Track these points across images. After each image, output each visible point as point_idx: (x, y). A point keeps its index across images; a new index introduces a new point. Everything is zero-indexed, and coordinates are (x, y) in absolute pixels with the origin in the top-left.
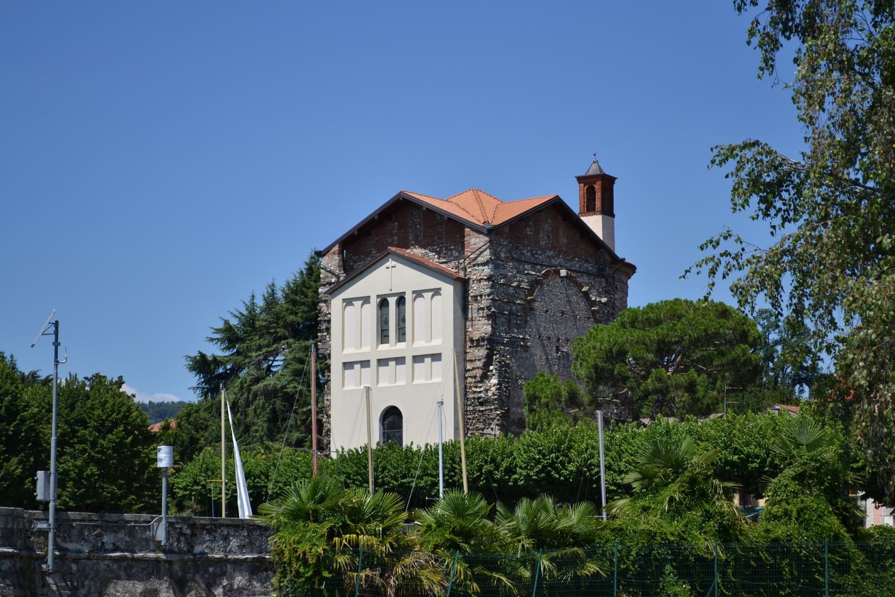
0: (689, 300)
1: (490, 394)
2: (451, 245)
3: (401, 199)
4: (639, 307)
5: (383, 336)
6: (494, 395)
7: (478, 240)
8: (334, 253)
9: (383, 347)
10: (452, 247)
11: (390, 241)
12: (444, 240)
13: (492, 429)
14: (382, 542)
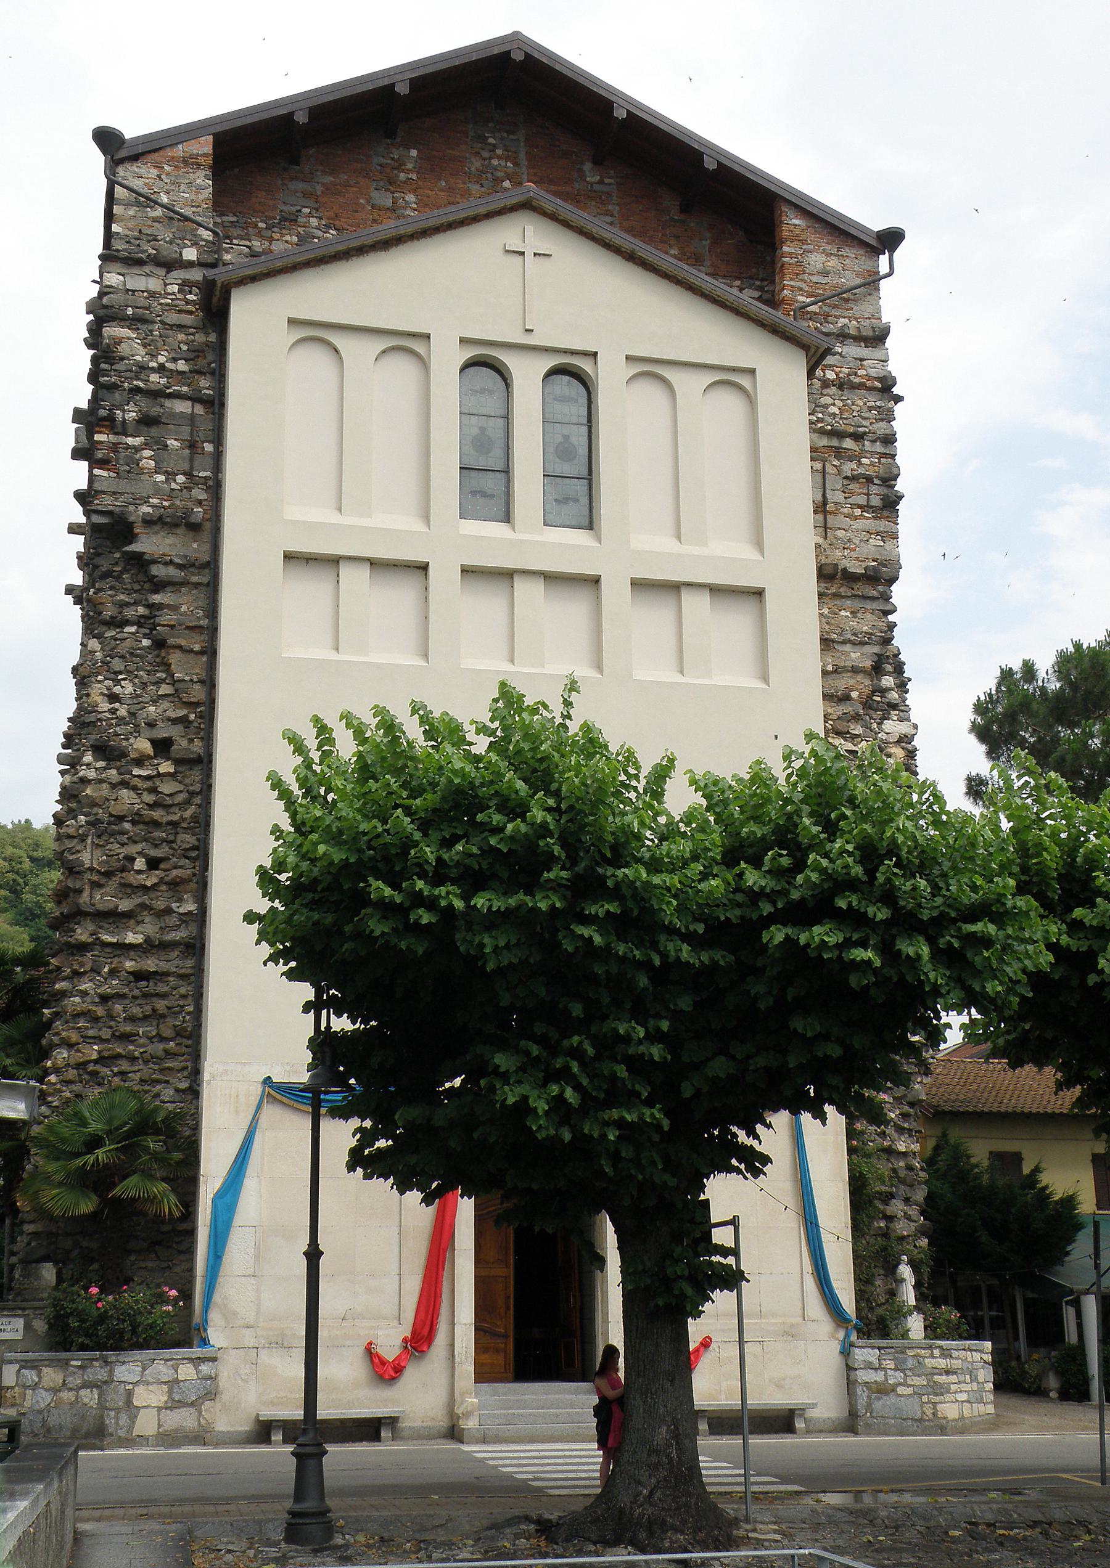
3: (518, 56)
7: (833, 263)
8: (190, 162)
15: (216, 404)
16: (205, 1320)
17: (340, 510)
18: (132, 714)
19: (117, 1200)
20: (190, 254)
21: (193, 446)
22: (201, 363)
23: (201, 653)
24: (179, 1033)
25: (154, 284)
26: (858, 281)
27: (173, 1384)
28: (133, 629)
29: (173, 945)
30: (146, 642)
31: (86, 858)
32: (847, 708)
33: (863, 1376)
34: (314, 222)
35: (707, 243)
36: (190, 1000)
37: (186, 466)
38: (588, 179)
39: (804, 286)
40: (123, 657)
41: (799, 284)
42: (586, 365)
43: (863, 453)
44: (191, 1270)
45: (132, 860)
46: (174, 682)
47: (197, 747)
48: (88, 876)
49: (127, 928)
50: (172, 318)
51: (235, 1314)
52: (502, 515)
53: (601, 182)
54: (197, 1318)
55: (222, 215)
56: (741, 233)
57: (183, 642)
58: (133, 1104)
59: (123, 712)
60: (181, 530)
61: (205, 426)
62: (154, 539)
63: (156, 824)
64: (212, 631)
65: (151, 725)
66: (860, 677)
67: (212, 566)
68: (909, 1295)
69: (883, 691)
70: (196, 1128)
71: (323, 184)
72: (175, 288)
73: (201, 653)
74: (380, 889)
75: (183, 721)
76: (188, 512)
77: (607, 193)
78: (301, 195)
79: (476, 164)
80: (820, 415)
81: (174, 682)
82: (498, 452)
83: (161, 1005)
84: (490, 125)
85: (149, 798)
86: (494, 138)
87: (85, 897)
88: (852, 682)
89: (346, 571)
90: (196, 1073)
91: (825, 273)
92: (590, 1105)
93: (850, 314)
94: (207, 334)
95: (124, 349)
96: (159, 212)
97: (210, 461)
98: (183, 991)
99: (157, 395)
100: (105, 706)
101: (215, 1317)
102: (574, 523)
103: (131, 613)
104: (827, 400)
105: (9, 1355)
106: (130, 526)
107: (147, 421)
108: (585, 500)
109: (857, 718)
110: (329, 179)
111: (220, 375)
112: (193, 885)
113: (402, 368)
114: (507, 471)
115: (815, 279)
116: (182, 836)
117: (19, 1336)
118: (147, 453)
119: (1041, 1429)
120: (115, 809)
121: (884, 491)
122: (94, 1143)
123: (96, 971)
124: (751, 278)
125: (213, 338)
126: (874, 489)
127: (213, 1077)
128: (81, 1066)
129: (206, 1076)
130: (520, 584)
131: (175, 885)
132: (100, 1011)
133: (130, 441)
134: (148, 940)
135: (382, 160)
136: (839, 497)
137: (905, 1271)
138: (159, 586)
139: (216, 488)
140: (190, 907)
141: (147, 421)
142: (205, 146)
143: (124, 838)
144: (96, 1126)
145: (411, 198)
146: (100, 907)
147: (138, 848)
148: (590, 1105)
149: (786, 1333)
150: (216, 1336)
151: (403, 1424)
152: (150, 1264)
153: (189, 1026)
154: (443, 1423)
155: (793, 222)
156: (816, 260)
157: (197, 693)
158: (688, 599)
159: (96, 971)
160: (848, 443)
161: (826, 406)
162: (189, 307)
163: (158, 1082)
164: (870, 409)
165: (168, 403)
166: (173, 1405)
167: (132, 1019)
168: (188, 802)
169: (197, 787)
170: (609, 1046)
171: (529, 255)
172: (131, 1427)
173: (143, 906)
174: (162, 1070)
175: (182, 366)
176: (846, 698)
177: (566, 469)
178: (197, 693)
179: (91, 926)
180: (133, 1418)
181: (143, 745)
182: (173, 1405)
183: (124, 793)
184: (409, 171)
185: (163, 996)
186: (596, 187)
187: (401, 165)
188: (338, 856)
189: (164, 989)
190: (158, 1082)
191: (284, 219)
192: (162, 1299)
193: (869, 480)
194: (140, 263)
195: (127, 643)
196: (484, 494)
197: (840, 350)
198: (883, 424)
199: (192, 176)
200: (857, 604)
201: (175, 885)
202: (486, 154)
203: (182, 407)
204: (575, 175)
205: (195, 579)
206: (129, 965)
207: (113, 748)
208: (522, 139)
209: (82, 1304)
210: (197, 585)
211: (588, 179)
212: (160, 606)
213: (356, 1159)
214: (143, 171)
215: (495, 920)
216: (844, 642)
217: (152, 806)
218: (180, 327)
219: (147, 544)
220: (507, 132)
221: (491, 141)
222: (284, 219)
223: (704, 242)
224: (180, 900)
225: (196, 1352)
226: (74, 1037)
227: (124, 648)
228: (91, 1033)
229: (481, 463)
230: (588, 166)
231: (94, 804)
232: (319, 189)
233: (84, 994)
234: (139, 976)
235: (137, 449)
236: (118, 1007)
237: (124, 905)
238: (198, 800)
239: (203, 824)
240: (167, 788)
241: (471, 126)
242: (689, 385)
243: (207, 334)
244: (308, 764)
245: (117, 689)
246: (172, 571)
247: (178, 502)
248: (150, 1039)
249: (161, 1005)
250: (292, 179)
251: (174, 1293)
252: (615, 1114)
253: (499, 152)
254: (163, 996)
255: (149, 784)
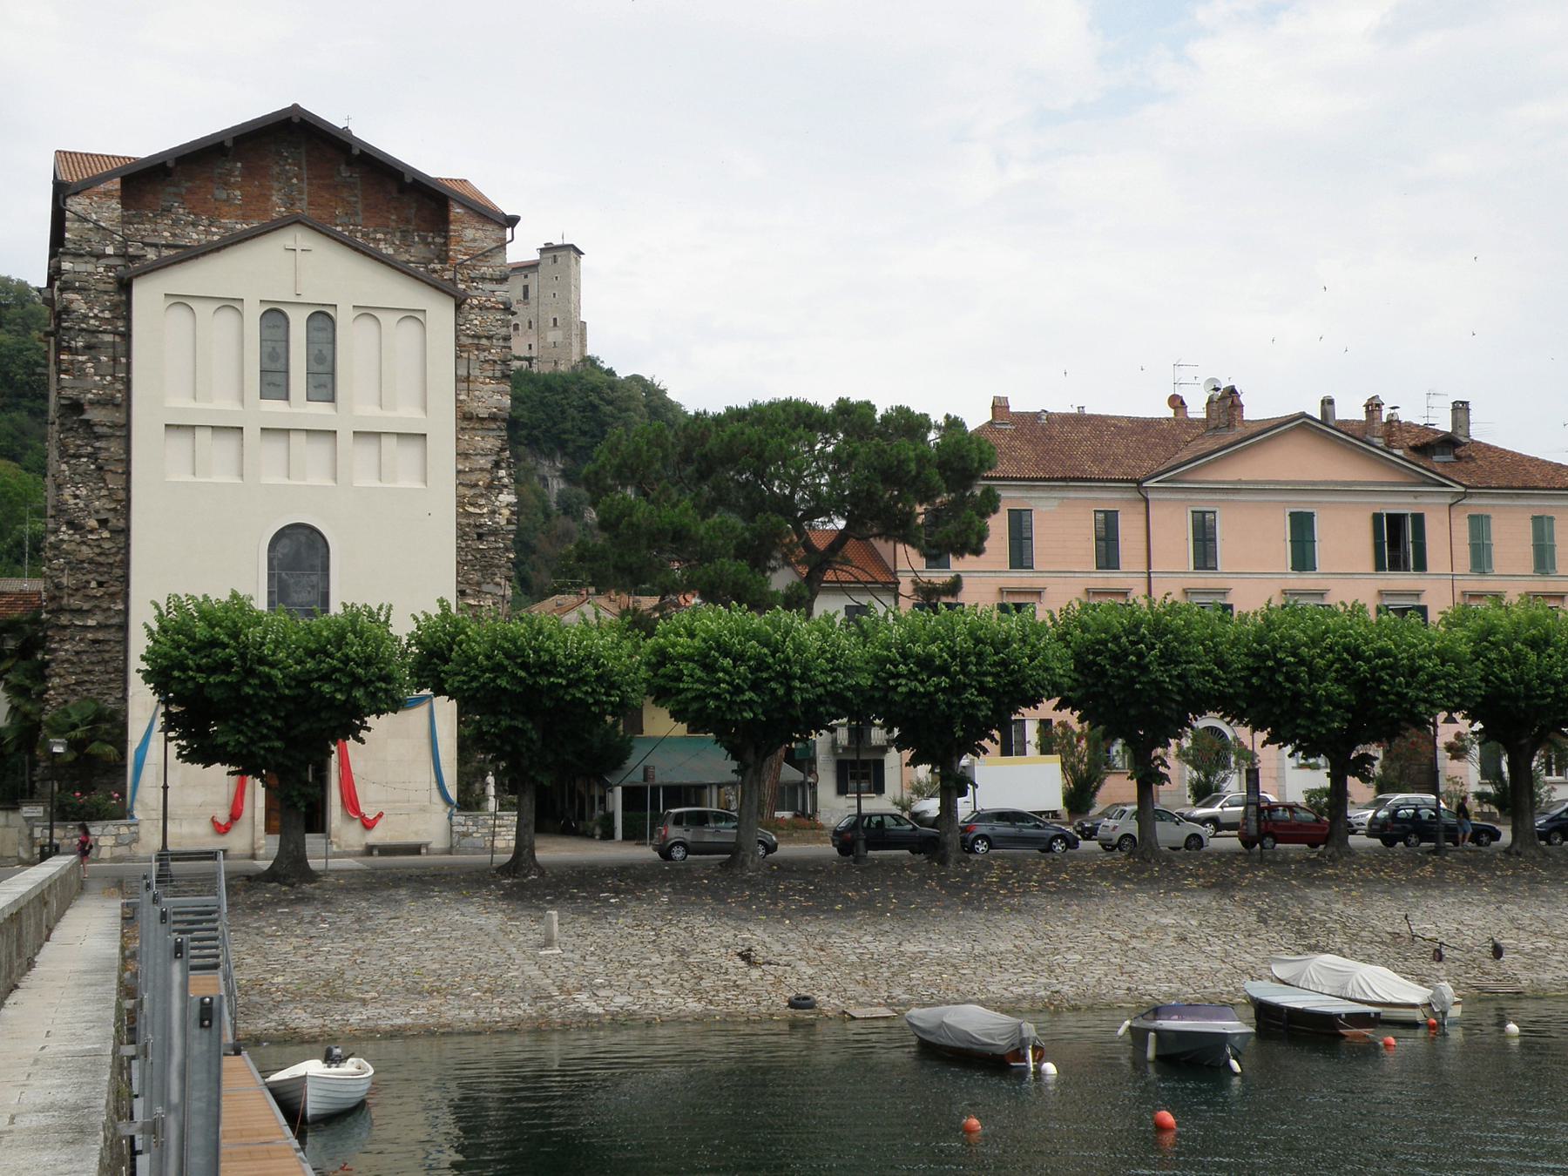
0: (873, 403)
1: (498, 518)
2: (376, 231)
3: (296, 120)
4: (1177, 402)
5: (274, 382)
6: (509, 522)
7: (479, 234)
8: (108, 194)
9: (275, 406)
10: (379, 236)
11: (224, 196)
12: (358, 219)
13: (498, 584)
14: (1376, 759)
15: (127, 336)
16: (132, 807)
17: (195, 398)
18: (87, 506)
19: (88, 755)
20: (110, 250)
21: (115, 360)
22: (118, 311)
23: (123, 473)
24: (116, 670)
25: (90, 268)
26: (494, 245)
27: (118, 835)
28: (85, 460)
29: (112, 626)
30: (92, 467)
31: (65, 581)
32: (477, 491)
33: (456, 829)
34: (181, 211)
35: (413, 211)
36: (121, 654)
37: (111, 371)
40: (80, 475)
42: (330, 311)
43: (492, 346)
44: (125, 784)
45: (89, 582)
46: (108, 489)
47: (121, 524)
48: (66, 590)
49: (88, 618)
50: (101, 287)
51: (147, 804)
52: (284, 396)
53: (351, 176)
54: (128, 806)
55: (127, 210)
57: (112, 468)
58: (93, 706)
59: (81, 505)
60: (110, 407)
61: (121, 349)
62: (95, 412)
63: (101, 564)
64: (127, 462)
65: (97, 512)
66: (484, 473)
67: (127, 426)
68: (491, 790)
69: (500, 479)
70: (126, 716)
71: (186, 188)
72: (102, 270)
73: (123, 473)
74: (176, 673)
75: (114, 510)
76: (113, 397)
79: (276, 169)
81: (108, 489)
82: (283, 361)
83: (107, 656)
85: (97, 550)
87: (65, 601)
88: (480, 476)
89: (198, 432)
90: (125, 690)
91: (474, 240)
92: (252, 741)
93: (488, 264)
94: (121, 295)
95: (74, 306)
96: (91, 225)
97: (124, 369)
98: (118, 649)
99: (94, 332)
100: (72, 501)
101: (137, 806)
102: (324, 398)
103: (83, 451)
104: (473, 316)
105: (37, 824)
106: (82, 405)
107: (89, 347)
108: (330, 386)
109: (482, 495)
110: (189, 184)
111: (128, 319)
112: (122, 595)
113: (228, 317)
114: (287, 372)
115: (468, 244)
116: (115, 570)
117: (41, 815)
118: (90, 365)
119: (569, 851)
120: (80, 557)
121: (504, 367)
122: (74, 727)
123: (72, 638)
125: (124, 298)
126: (498, 367)
127: (134, 694)
128: (67, 686)
129: (130, 694)
130: (292, 436)
131: (112, 596)
132: (75, 659)
133: (80, 358)
134: (98, 623)
135: (220, 171)
136: (477, 372)
137: (491, 779)
138: (99, 437)
139: (128, 383)
140: (121, 607)
141: (89, 347)
143: (84, 571)
144: (75, 718)
145: (238, 193)
146: (73, 607)
147: (92, 576)
148: (252, 741)
149: (421, 810)
150: (138, 814)
151: (230, 853)
152: (105, 781)
153: (121, 666)
154: (249, 852)
155: (456, 210)
156: (469, 233)
157: (121, 495)
158: (384, 439)
159: (72, 638)
160: (484, 341)
161: (472, 320)
162: (110, 280)
163: (106, 694)
164: (497, 320)
165: (100, 336)
166: (117, 845)
167: (92, 663)
168: (116, 554)
169: (122, 545)
170: (260, 723)
171: (298, 251)
172: (98, 855)
173: (96, 606)
174: (108, 688)
175: (107, 315)
176: (476, 485)
177: (320, 369)
178: (121, 495)
179: (68, 616)
180: (99, 851)
181: (93, 523)
182: (117, 845)
183: (84, 548)
184: (237, 176)
185: (108, 652)
186: (348, 180)
188: (165, 663)
189: (108, 648)
190: (106, 694)
191: (163, 210)
192: (111, 798)
193: (495, 362)
194: (81, 256)
195: (83, 467)
196: (274, 384)
198: (505, 329)
199: (109, 203)
200: (485, 433)
201: (112, 596)
202: (281, 163)
203: (108, 338)
205: (118, 434)
206: (89, 636)
207: (77, 525)
209: (73, 800)
210: (119, 437)
212: (100, 448)
213: (179, 755)
214: (81, 201)
215: (217, 685)
216: (476, 455)
217: (99, 555)
218: (106, 292)
219: (93, 415)
221: (285, 154)
222: (163, 210)
224: (115, 603)
225: (128, 821)
226: (62, 672)
227: (81, 469)
228: (71, 670)
229: (273, 367)
230: (343, 167)
231: (68, 553)
232: (184, 191)
233: (66, 651)
234: (95, 642)
235: (84, 363)
236: (84, 657)
237: (86, 607)
238: (123, 551)
239: (126, 564)
240: (106, 545)
242: (389, 320)
243: (121, 295)
244: (161, 614)
245: (78, 492)
246: (105, 430)
247: (107, 391)
248: (102, 673)
249: (107, 656)
251: (116, 795)
252: (262, 744)
253: (290, 161)
254: (108, 652)
255: (97, 543)
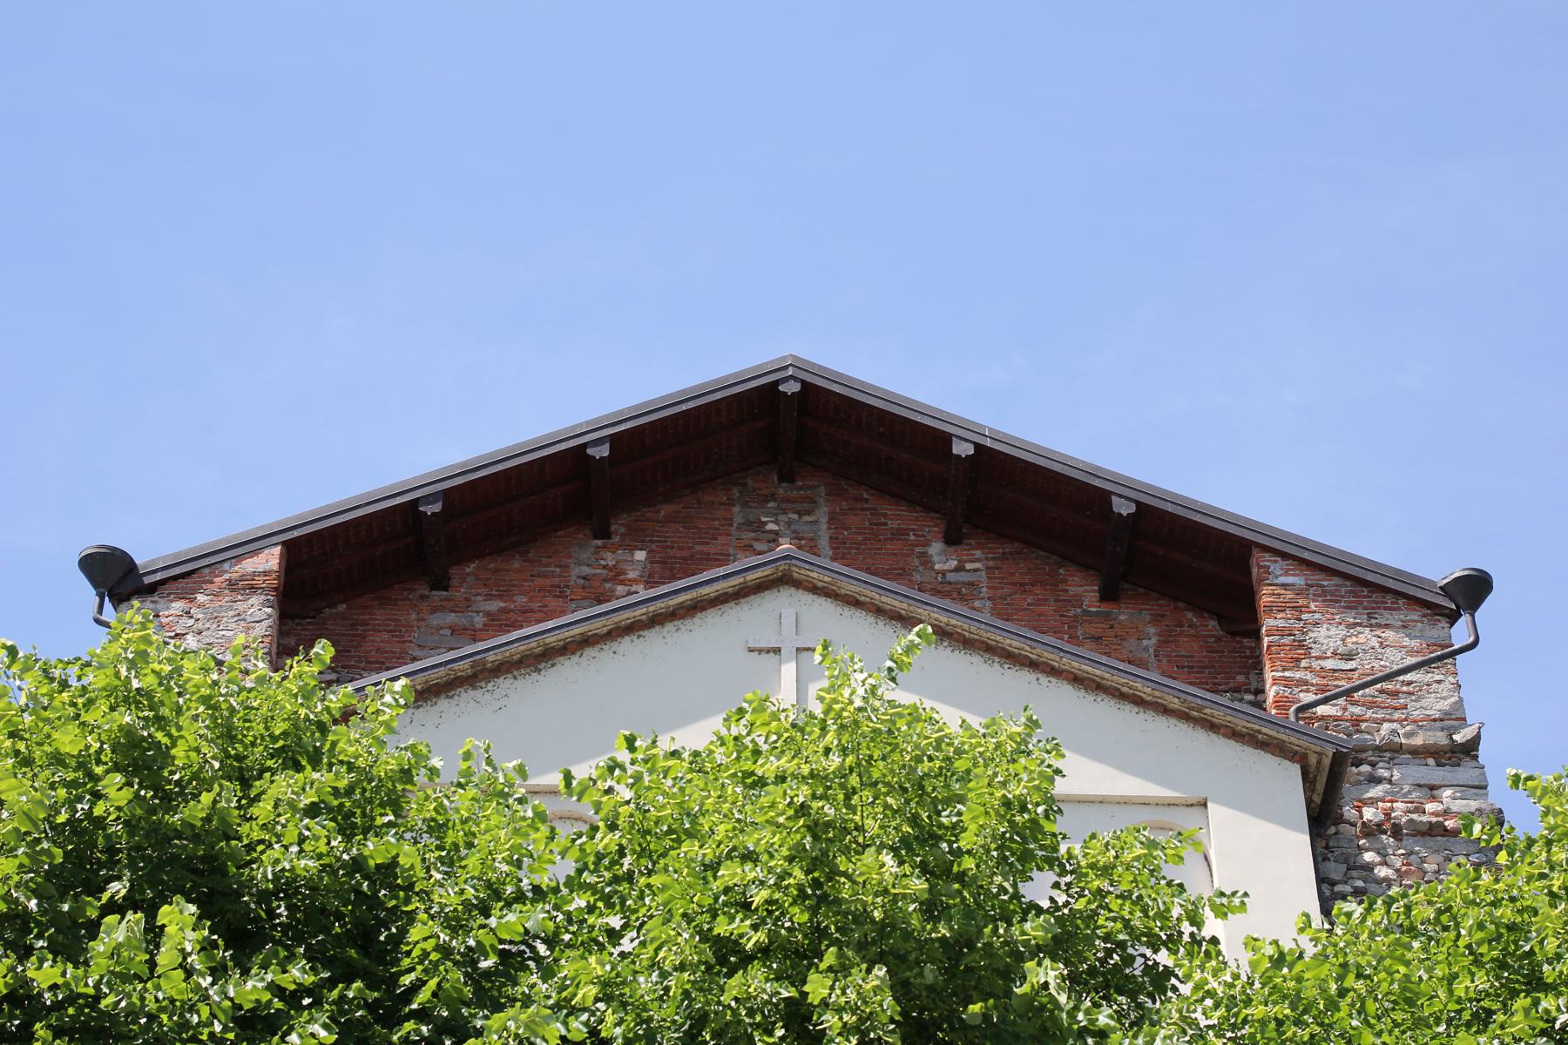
7: (1366, 637)
8: (246, 586)
35: (1151, 643)
38: (937, 567)
39: (1309, 676)
41: (1298, 675)
53: (960, 569)
56: (1212, 624)
77: (972, 584)
78: (448, 632)
80: (1360, 883)
84: (771, 505)
86: (776, 522)
110: (495, 605)
115: (1329, 664)
124: (1237, 690)
135: (587, 570)
142: (270, 560)
156: (1328, 635)
186: (951, 577)
187: (619, 574)
197: (1386, 774)
199: (240, 606)
204: (916, 562)
208: (824, 520)
211: (937, 567)
220: (800, 513)
221: (771, 527)
223: (1145, 642)
230: (936, 548)
241: (736, 509)
250: (434, 610)
